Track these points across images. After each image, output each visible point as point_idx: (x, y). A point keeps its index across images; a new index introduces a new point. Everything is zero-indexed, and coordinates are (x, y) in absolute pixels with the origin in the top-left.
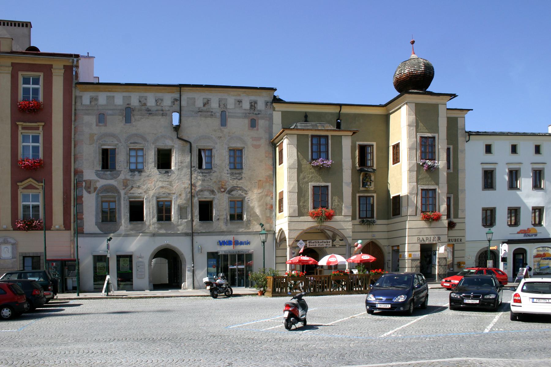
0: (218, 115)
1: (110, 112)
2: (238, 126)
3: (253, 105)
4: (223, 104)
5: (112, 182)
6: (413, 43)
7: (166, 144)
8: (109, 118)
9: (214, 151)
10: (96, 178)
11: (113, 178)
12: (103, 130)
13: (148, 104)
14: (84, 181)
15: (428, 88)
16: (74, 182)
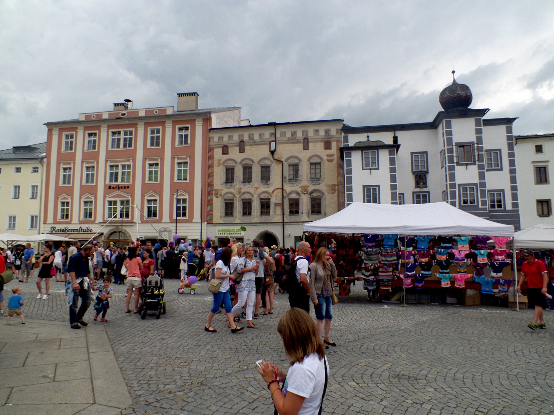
0: (302, 141)
2: (317, 148)
3: (327, 132)
4: (305, 132)
6: (453, 72)
7: (267, 163)
8: (230, 149)
12: (226, 157)
14: (215, 190)
15: (469, 105)
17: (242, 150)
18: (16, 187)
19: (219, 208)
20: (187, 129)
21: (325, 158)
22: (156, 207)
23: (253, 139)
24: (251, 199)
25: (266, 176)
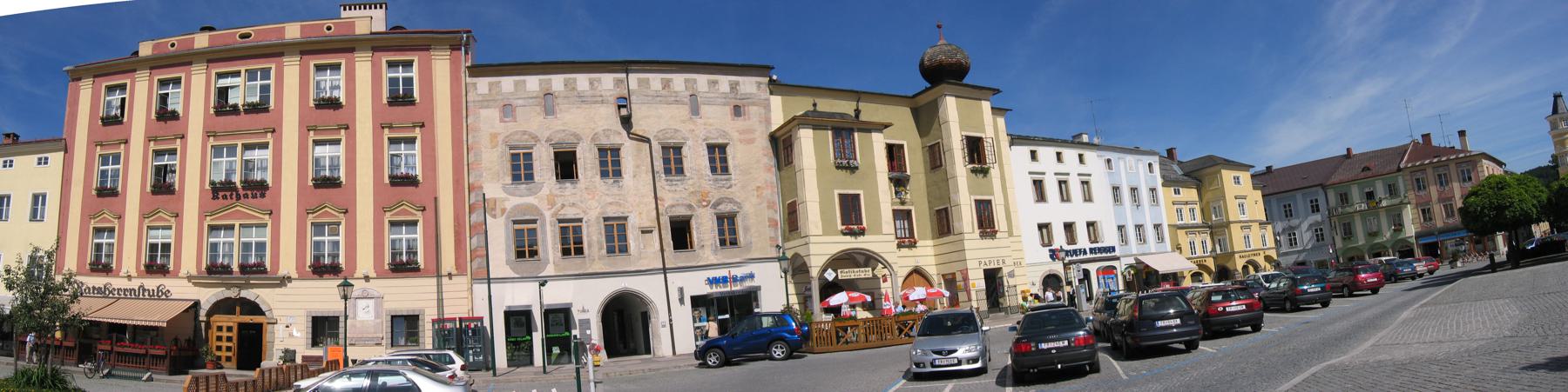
0: (687, 100)
1: (520, 102)
5: (531, 200)
9: (685, 151)
10: (503, 195)
11: (531, 193)
12: (511, 127)
13: (580, 89)
16: (472, 206)
17: (549, 111)
18: (1041, 227)
19: (503, 240)
20: (408, 65)
21: (735, 135)
22: (415, 240)
23: (574, 89)
24: (690, 217)
25: (610, 162)
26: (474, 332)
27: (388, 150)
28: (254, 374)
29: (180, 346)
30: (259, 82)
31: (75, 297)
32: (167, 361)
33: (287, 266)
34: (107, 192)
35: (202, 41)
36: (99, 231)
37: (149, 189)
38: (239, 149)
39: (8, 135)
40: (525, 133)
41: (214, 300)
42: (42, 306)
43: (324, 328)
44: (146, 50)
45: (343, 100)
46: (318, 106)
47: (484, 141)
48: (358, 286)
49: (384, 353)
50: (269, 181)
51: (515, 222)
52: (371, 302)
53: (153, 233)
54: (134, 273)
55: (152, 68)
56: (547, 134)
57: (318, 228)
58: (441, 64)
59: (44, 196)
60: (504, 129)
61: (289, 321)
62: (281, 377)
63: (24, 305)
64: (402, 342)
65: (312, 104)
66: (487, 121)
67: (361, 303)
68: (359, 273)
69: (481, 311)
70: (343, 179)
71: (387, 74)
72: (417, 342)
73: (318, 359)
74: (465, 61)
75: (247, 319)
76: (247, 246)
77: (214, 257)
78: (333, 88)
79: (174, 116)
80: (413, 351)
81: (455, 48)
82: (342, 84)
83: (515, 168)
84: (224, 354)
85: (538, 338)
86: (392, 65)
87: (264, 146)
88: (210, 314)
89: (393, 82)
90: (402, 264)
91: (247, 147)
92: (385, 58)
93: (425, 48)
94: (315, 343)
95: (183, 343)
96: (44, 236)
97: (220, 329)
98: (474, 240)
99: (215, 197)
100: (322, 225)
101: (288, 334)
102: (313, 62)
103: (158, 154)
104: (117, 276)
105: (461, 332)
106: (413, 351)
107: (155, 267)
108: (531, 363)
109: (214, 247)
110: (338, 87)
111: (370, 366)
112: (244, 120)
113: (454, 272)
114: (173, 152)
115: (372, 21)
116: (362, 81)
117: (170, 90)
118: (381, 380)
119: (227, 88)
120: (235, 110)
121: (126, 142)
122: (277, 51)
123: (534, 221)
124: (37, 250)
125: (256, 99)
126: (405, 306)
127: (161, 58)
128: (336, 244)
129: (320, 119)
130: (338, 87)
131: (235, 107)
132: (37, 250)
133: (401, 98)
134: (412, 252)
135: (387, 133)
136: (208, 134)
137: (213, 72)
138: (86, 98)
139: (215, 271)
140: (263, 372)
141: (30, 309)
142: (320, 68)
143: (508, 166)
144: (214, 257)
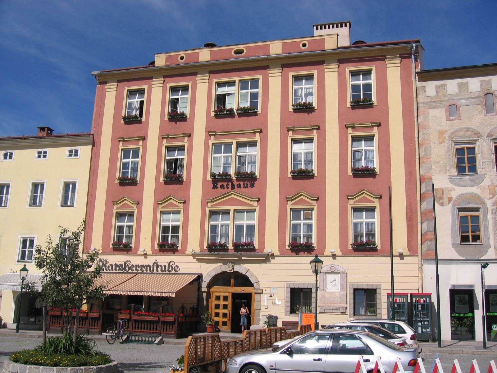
1: (463, 102)
5: (474, 190)
10: (450, 186)
11: (475, 183)
12: (456, 124)
16: (423, 196)
26: (423, 306)
27: (351, 147)
28: (242, 336)
29: (184, 314)
30: (250, 91)
31: (98, 272)
32: (175, 326)
33: (271, 245)
34: (128, 181)
35: (205, 55)
36: (120, 215)
37: (162, 179)
38: (234, 146)
39: (43, 129)
40: (468, 129)
41: (213, 274)
42: (68, 281)
43: (300, 297)
44: (160, 61)
45: (315, 105)
46: (296, 111)
47: (433, 137)
48: (327, 262)
49: (346, 320)
50: (257, 174)
51: (460, 210)
52: (337, 277)
53: (165, 217)
54: (149, 252)
55: (165, 77)
56: (488, 130)
57: (296, 213)
58: (393, 70)
59: (74, 185)
60: (450, 127)
61: (272, 291)
62: (264, 338)
63: (53, 280)
64: (363, 312)
65: (291, 108)
66: (435, 120)
67: (330, 277)
68: (328, 252)
69: (430, 288)
70: (315, 172)
71: (350, 82)
72: (375, 312)
73: (295, 324)
74: (415, 68)
75: (239, 290)
76: (239, 228)
77: (214, 237)
78: (307, 95)
79: (183, 118)
80: (370, 320)
81: (405, 56)
82: (315, 91)
83: (460, 161)
84: (221, 319)
85: (479, 315)
86: (354, 74)
87: (253, 144)
88: (210, 285)
89: (355, 88)
90: (363, 244)
91: (240, 145)
92: (349, 68)
93: (381, 58)
94: (293, 311)
95: (188, 311)
96: (72, 219)
97: (218, 298)
98: (425, 225)
99: (215, 187)
100: (299, 210)
101: (271, 304)
102: (292, 73)
103: (170, 149)
104: (136, 254)
105: (412, 306)
106: (370, 320)
107: (167, 246)
108: (473, 338)
109: (214, 229)
110: (311, 94)
111: (337, 330)
112: (237, 122)
113: (406, 252)
114: (181, 148)
115: (338, 38)
116: (330, 88)
117: (180, 96)
118: (342, 342)
119: (224, 96)
120: (231, 113)
121: (144, 139)
122: (263, 65)
123: (477, 209)
124: (65, 231)
125: (247, 105)
126: (365, 281)
127: (173, 69)
128: (310, 227)
129: (297, 119)
130: (311, 94)
131: (231, 110)
132: (65, 231)
133: (362, 102)
134: (371, 234)
135: (350, 133)
136: (210, 133)
137: (214, 82)
138: (111, 100)
139: (215, 249)
140: (249, 334)
141: (58, 284)
142: (297, 79)
143: (454, 159)
144: (214, 237)
